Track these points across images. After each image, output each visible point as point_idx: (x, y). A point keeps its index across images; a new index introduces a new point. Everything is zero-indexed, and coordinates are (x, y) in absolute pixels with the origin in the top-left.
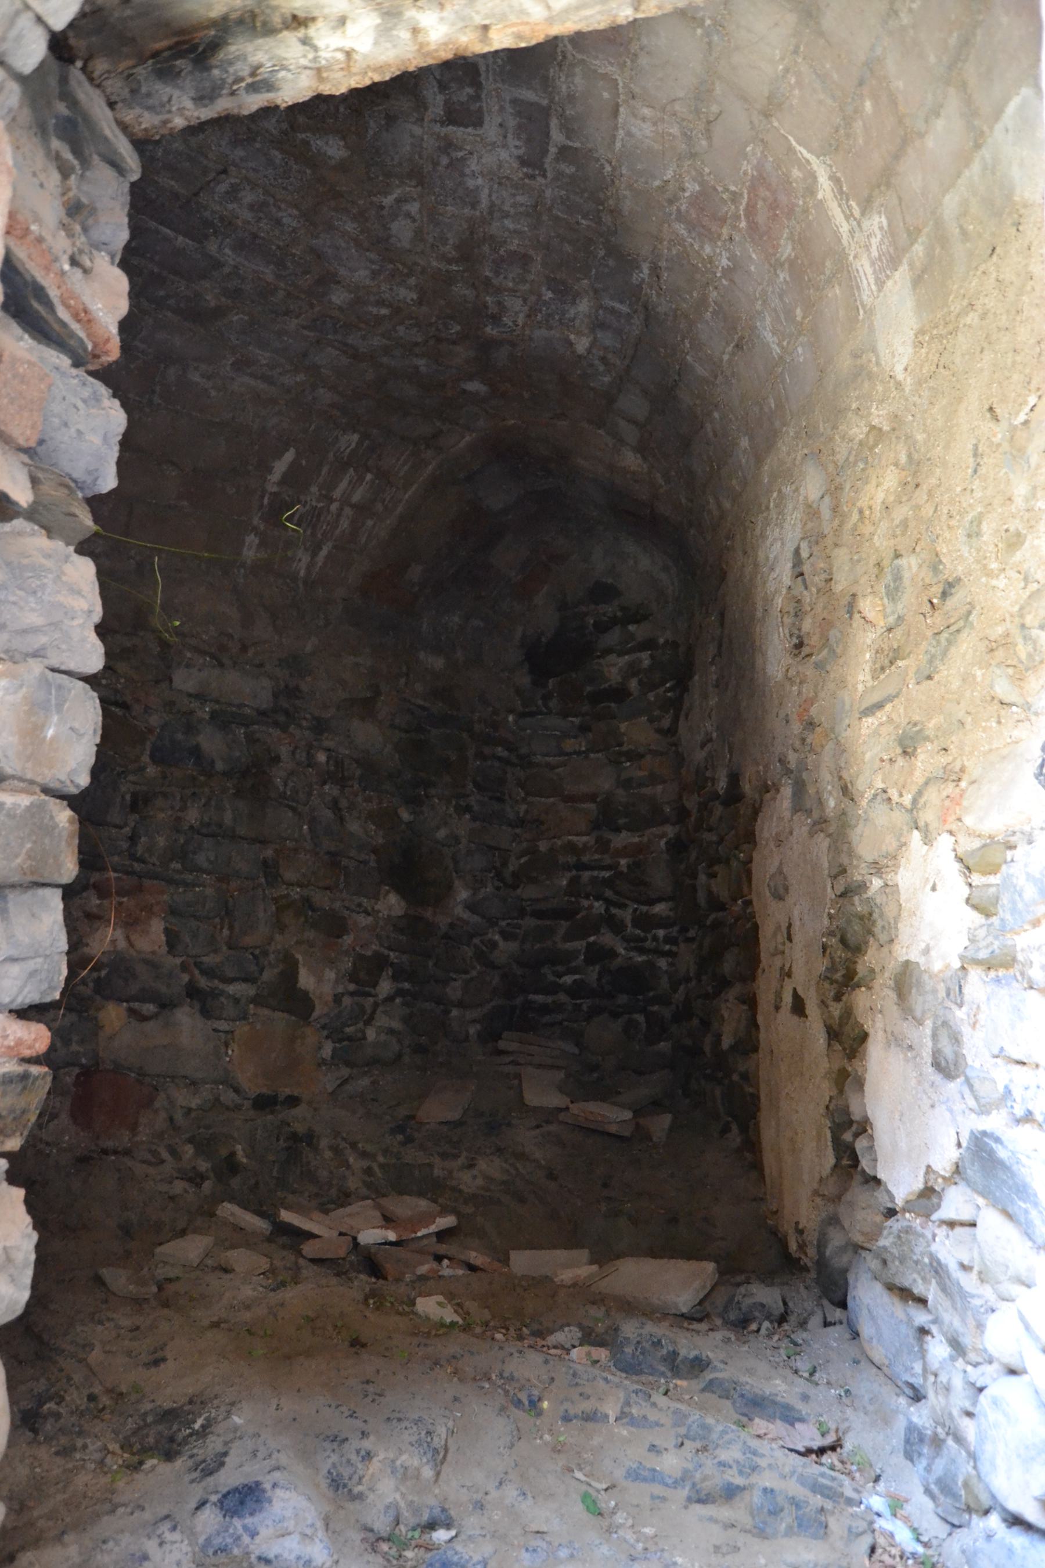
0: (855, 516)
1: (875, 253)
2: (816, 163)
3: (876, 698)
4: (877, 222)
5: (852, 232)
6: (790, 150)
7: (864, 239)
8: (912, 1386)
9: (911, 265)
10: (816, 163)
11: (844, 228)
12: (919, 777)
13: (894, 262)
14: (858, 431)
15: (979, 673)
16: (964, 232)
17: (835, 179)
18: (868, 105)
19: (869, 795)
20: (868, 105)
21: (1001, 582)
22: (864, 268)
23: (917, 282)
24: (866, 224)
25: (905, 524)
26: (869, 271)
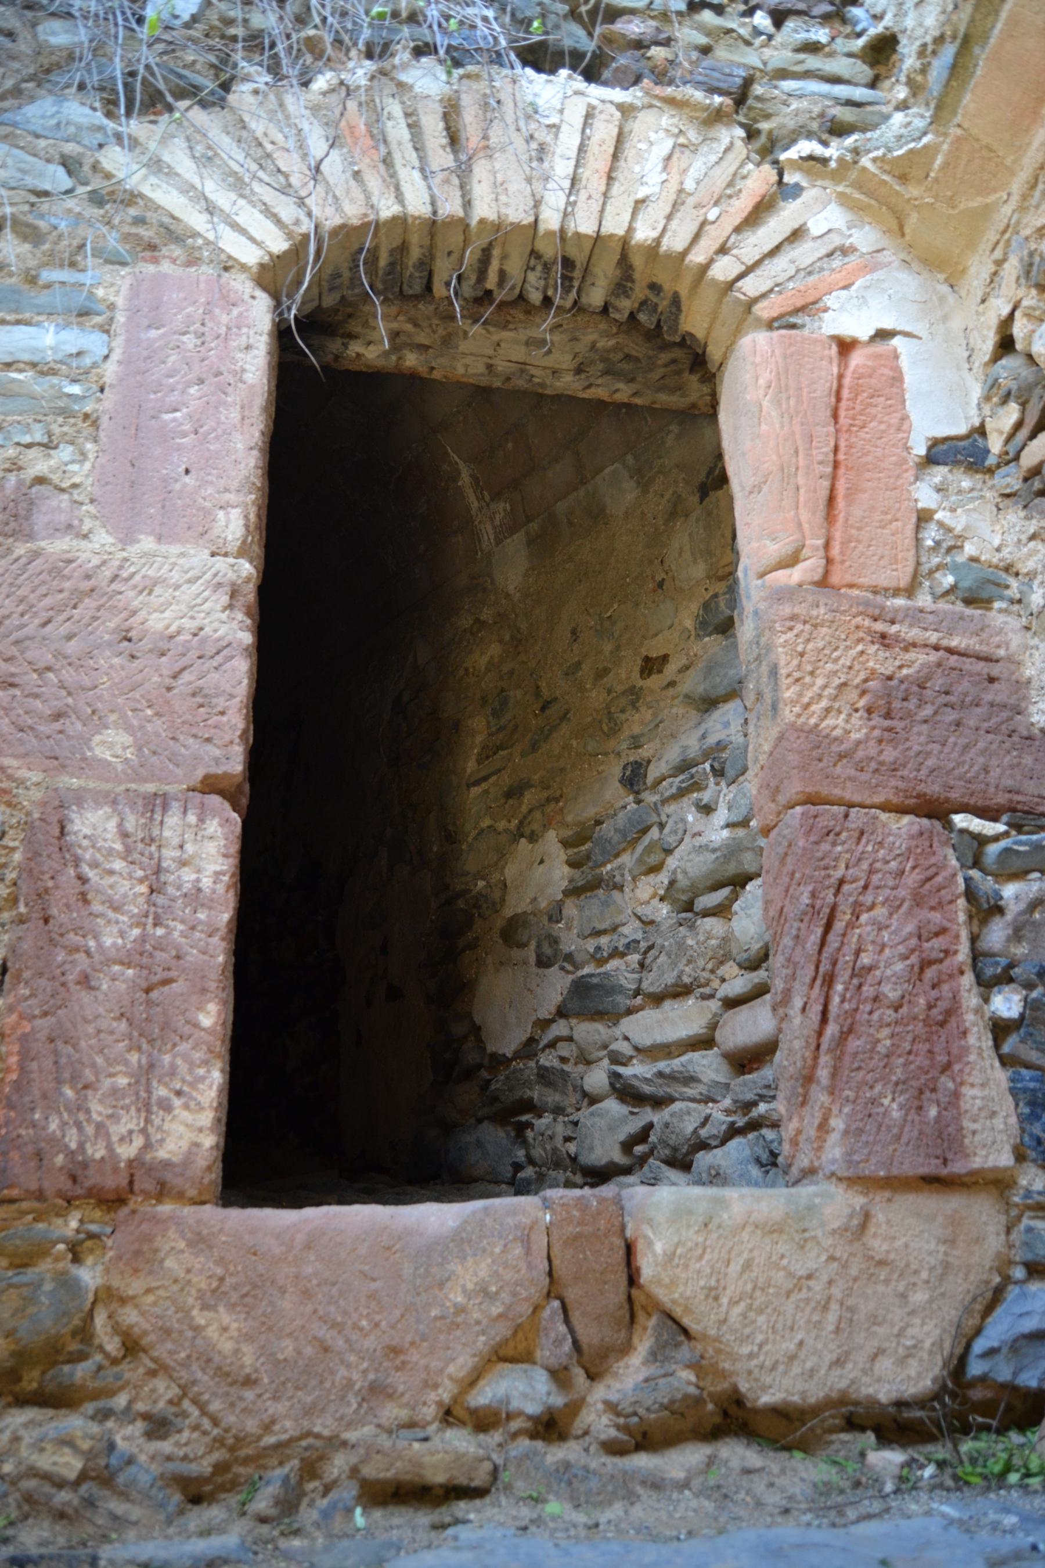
0: (461, 672)
1: (497, 522)
2: (461, 465)
3: (482, 774)
4: (501, 508)
5: (480, 509)
6: (446, 453)
7: (487, 516)
8: (887, 646)
9: (527, 533)
10: (461, 465)
11: (475, 505)
12: (524, 809)
13: (512, 530)
14: (466, 622)
15: (574, 743)
16: (570, 523)
17: (473, 476)
18: (510, 445)
19: (473, 834)
20: (510, 445)
21: (594, 694)
22: (487, 533)
23: (530, 543)
24: (493, 506)
25: (511, 673)
26: (491, 531)
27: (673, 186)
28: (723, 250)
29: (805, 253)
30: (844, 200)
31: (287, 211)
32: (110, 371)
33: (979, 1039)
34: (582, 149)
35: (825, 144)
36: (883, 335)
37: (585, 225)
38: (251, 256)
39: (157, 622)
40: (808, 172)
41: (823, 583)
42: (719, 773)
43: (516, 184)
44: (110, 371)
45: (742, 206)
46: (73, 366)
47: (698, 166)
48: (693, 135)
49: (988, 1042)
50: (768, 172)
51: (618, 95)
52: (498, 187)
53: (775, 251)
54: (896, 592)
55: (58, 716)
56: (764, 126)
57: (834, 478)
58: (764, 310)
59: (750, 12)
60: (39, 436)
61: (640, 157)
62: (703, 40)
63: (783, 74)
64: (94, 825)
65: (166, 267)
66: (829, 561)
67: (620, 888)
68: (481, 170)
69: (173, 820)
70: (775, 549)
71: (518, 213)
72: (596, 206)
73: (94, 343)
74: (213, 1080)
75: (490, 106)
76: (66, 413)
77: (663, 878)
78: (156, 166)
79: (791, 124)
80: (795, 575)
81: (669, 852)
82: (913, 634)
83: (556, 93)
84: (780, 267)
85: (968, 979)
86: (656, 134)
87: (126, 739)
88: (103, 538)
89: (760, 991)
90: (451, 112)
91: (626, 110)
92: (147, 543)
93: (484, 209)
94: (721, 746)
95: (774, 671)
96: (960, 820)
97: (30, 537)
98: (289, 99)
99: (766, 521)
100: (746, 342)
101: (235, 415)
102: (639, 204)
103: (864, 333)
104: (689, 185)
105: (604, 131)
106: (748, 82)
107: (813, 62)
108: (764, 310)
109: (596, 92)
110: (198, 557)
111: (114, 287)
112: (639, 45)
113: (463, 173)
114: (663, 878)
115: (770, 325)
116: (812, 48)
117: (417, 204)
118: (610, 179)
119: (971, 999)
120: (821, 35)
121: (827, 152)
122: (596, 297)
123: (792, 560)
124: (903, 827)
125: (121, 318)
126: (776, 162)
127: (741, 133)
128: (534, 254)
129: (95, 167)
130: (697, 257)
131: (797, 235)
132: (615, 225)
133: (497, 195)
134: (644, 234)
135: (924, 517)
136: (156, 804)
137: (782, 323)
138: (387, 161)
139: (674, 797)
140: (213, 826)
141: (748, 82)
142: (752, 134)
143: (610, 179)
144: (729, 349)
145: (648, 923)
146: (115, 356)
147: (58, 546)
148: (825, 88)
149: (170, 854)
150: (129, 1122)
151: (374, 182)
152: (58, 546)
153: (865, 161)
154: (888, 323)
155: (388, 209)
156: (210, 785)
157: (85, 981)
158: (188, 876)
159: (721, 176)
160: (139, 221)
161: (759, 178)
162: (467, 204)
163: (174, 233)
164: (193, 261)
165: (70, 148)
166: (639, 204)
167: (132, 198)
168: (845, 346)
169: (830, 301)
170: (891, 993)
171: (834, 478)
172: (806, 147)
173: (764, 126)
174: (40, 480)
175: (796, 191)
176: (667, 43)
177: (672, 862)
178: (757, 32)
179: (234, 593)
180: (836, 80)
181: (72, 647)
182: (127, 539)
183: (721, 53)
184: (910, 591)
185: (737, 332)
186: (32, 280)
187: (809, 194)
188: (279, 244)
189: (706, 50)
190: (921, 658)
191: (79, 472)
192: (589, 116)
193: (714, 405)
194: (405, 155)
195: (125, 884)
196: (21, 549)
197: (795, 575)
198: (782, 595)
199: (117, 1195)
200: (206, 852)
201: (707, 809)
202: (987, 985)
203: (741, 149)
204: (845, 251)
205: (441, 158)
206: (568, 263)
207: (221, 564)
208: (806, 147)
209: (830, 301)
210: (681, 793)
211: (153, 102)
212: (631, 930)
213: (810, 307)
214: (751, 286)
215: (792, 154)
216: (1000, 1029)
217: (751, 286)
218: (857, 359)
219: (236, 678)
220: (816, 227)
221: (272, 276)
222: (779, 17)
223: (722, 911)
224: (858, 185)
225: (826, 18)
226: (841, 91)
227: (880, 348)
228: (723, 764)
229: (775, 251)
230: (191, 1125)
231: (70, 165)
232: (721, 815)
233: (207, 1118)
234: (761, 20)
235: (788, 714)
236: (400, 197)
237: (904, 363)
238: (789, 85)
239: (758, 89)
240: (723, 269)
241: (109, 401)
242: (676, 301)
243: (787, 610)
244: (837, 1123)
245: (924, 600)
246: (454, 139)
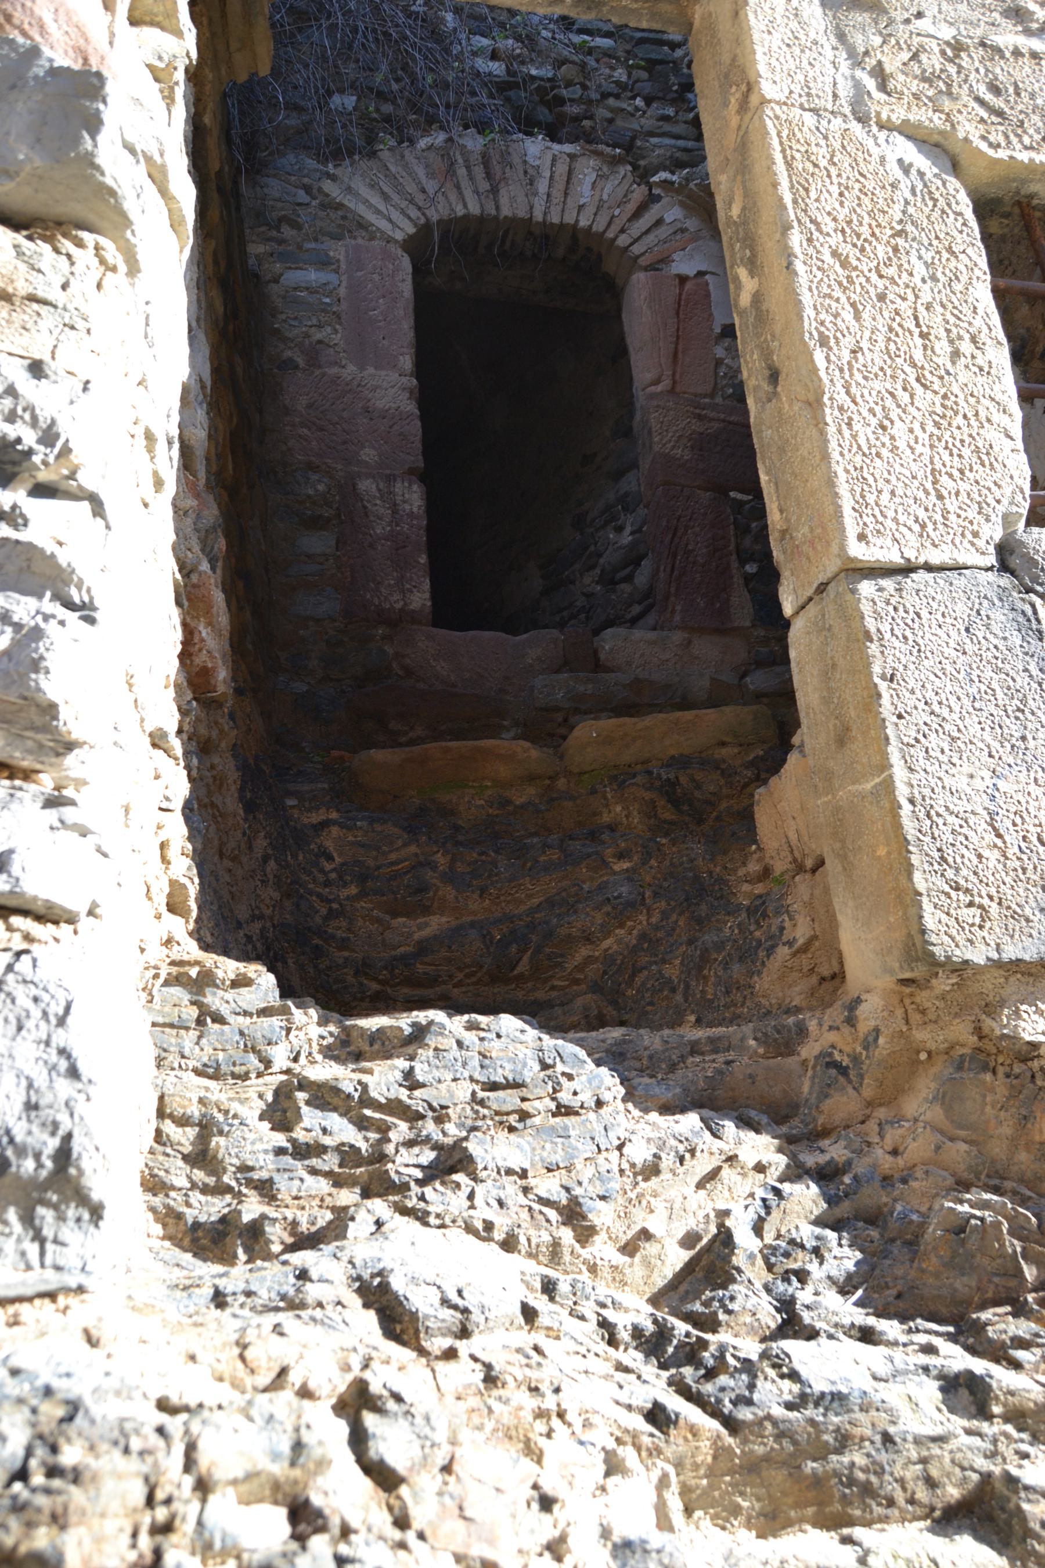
27: (597, 198)
28: (622, 231)
29: (663, 232)
30: (682, 204)
31: (414, 213)
32: (342, 292)
33: (738, 580)
34: (551, 178)
35: (673, 173)
36: (701, 274)
37: (556, 220)
38: (399, 236)
39: (380, 404)
40: (664, 189)
41: (672, 391)
42: (625, 509)
43: (521, 198)
44: (342, 292)
45: (631, 207)
46: (323, 289)
47: (609, 187)
48: (605, 169)
49: (742, 581)
50: (644, 189)
51: (568, 148)
52: (512, 199)
53: (648, 231)
54: (705, 396)
55: (344, 443)
56: (642, 163)
57: (677, 344)
58: (643, 261)
59: (634, 98)
60: (315, 322)
61: (581, 183)
62: (609, 115)
63: (652, 134)
64: (367, 486)
65: (360, 241)
66: (674, 382)
67: (573, 582)
68: (503, 192)
69: (398, 485)
70: (649, 376)
71: (522, 213)
72: (559, 208)
73: (332, 278)
74: (427, 585)
75: (505, 157)
76: (324, 311)
77: (598, 571)
78: (349, 190)
79: (655, 161)
80: (659, 388)
81: (600, 556)
82: (713, 414)
83: (535, 148)
84: (651, 239)
85: (734, 557)
86: (588, 170)
87: (373, 452)
88: (351, 368)
89: (650, 607)
90: (486, 160)
91: (572, 157)
92: (371, 370)
93: (506, 211)
94: (626, 494)
95: (650, 432)
96: (732, 494)
97: (320, 367)
98: (407, 153)
99: (646, 367)
100: (634, 277)
101: (402, 312)
102: (581, 207)
103: (691, 273)
104: (605, 197)
105: (562, 168)
106: (633, 139)
107: (667, 127)
108: (643, 261)
109: (556, 147)
110: (394, 376)
111: (338, 251)
112: (577, 119)
113: (494, 191)
114: (598, 571)
115: (646, 269)
116: (665, 118)
117: (474, 209)
118: (566, 194)
119: (735, 565)
120: (670, 111)
121: (674, 178)
122: (560, 253)
123: (657, 382)
124: (705, 496)
125: (343, 266)
126: (648, 183)
127: (629, 168)
128: (530, 233)
129: (320, 189)
130: (610, 235)
131: (659, 222)
132: (569, 218)
133: (512, 203)
134: (583, 223)
135: (719, 362)
136: (391, 479)
137: (651, 268)
138: (458, 187)
139: (603, 527)
140: (415, 487)
141: (633, 139)
142: (635, 167)
143: (566, 194)
144: (627, 280)
145: (588, 596)
146: (344, 284)
147: (334, 371)
148: (673, 142)
149: (399, 498)
150: (396, 596)
151: (453, 197)
152: (334, 371)
153: (692, 185)
154: (703, 268)
155: (460, 211)
156: (411, 471)
157: (371, 546)
158: (407, 507)
159: (621, 192)
160: (344, 218)
161: (639, 193)
162: (497, 208)
163: (363, 225)
164: (372, 238)
165: (306, 180)
166: (581, 207)
167: (340, 206)
168: (683, 279)
169: (675, 256)
170: (700, 560)
171: (677, 344)
172: (664, 175)
173: (642, 163)
174: (320, 342)
175: (657, 199)
176: (591, 118)
177: (602, 561)
178: (637, 109)
179: (411, 392)
180: (678, 137)
181: (345, 414)
182: (362, 368)
183: (619, 123)
184: (712, 395)
185: (630, 273)
186: (300, 247)
187: (664, 201)
188: (411, 230)
189: (611, 121)
190: (716, 425)
191: (337, 338)
192: (554, 160)
193: (619, 310)
194: (465, 183)
195: (381, 509)
196: (317, 372)
197: (659, 388)
198: (652, 396)
199: (398, 621)
200: (413, 498)
201: (619, 529)
202: (742, 562)
203: (630, 177)
204: (683, 230)
205: (484, 186)
206: (547, 237)
207: (404, 380)
208: (664, 175)
209: (675, 256)
210: (607, 523)
211: (337, 156)
212: (581, 602)
213: (666, 260)
214: (636, 249)
215: (655, 179)
216: (748, 578)
217: (636, 249)
218: (688, 286)
219: (416, 427)
220: (669, 218)
221: (410, 245)
222: (648, 101)
223: (629, 579)
224: (689, 197)
225: (673, 102)
226: (681, 143)
227: (699, 280)
228: (627, 502)
229: (648, 231)
230: (420, 599)
231: (308, 189)
232: (628, 529)
233: (427, 595)
234: (639, 102)
235: (656, 448)
236: (465, 206)
237: (711, 288)
238: (654, 140)
239: (639, 143)
240: (623, 241)
241: (344, 306)
242: (599, 256)
243: (655, 403)
244: (678, 608)
245: (719, 400)
246: (489, 175)
